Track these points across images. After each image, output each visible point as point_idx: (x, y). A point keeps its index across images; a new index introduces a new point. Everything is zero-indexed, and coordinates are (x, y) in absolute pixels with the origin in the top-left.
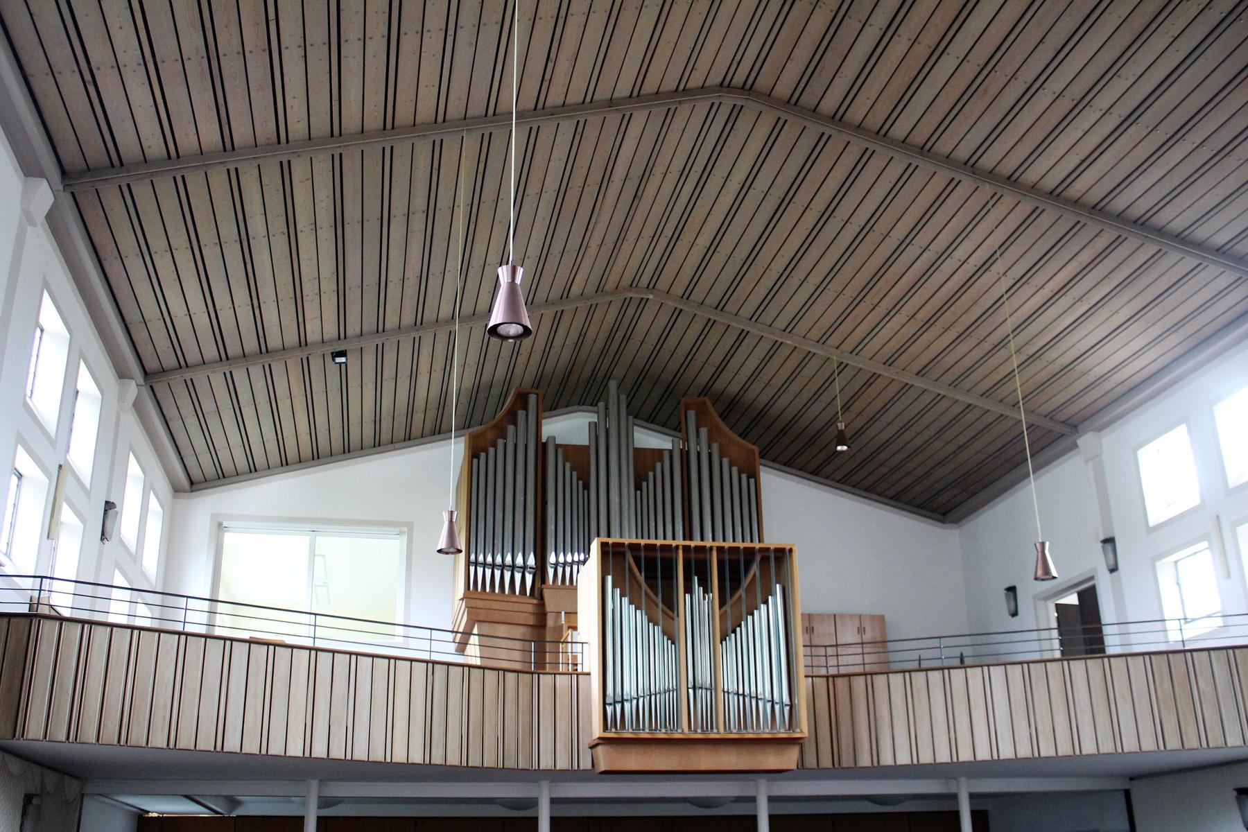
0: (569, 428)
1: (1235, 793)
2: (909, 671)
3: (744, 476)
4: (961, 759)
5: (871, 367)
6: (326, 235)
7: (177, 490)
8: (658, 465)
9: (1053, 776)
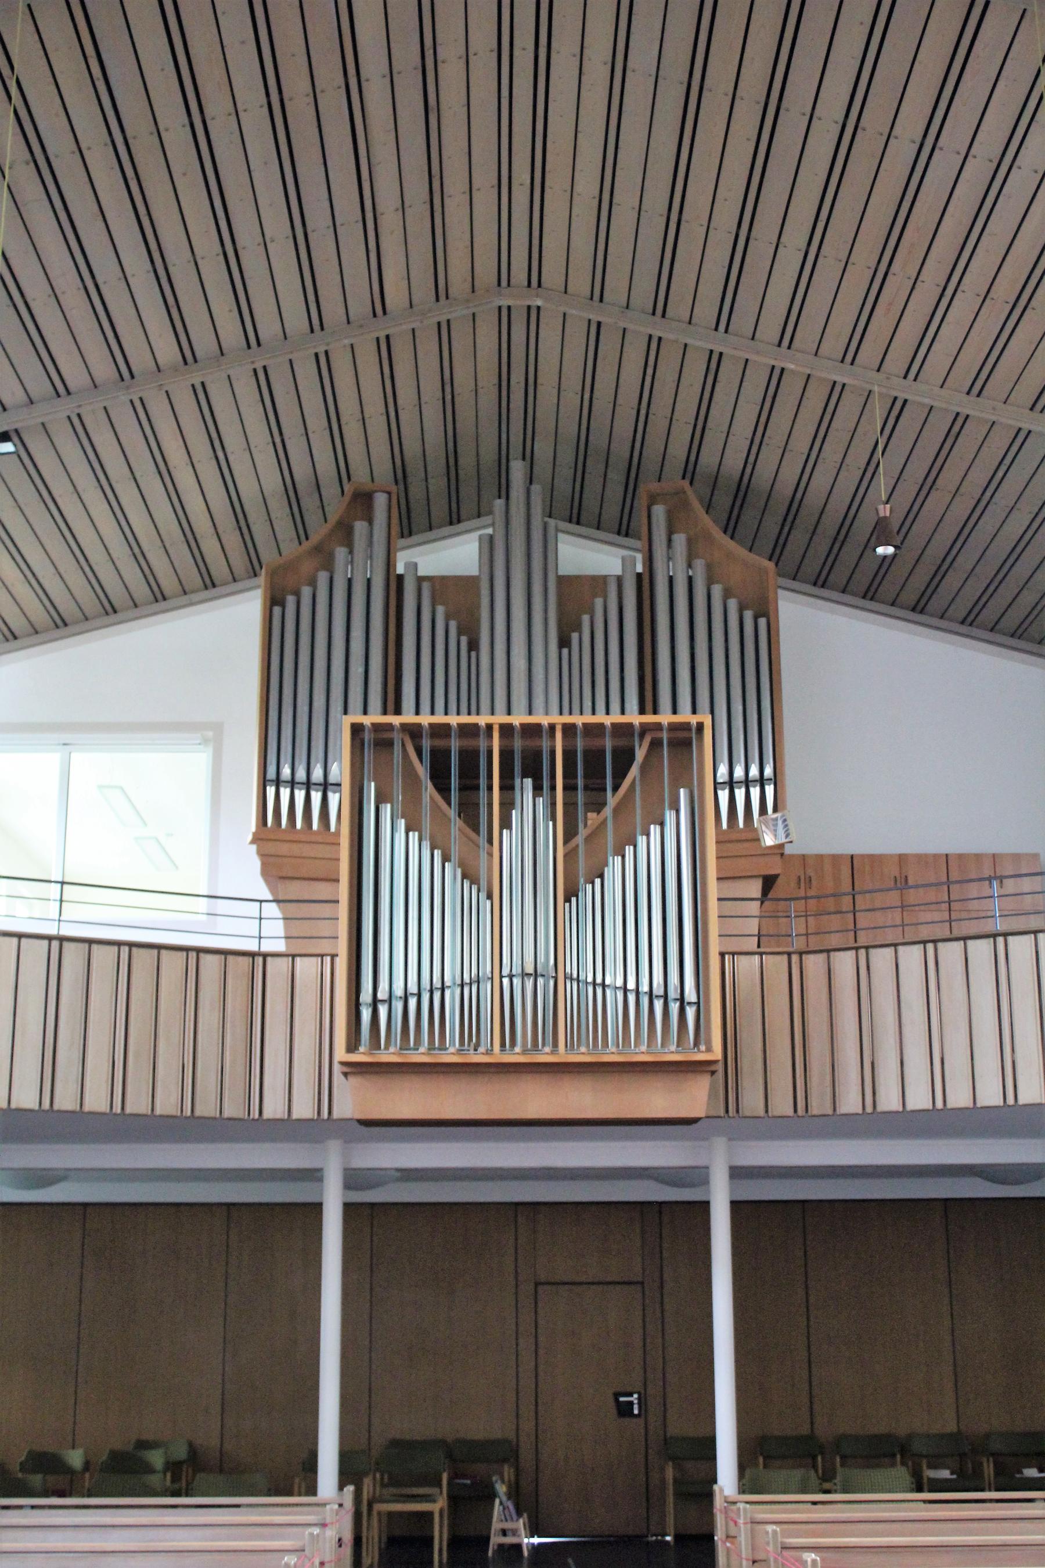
0: (456, 554)
3: (748, 615)
4: (1022, 1100)
5: (954, 401)
8: (599, 602)
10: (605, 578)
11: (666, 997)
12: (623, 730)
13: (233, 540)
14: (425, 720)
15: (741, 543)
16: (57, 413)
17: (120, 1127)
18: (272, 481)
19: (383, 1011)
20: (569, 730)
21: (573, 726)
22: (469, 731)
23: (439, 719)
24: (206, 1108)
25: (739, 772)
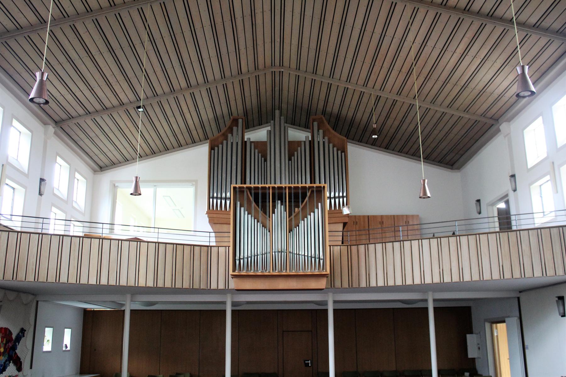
0: (259, 134)
1: (557, 299)
2: (403, 241)
3: (339, 152)
6: (107, 55)
7: (95, 171)
8: (299, 148)
9: (475, 291)
10: (301, 142)
11: (315, 257)
12: (304, 188)
13: (200, 131)
14: (252, 186)
15: (338, 133)
16: (154, 102)
17: (174, 291)
18: (211, 116)
19: (242, 261)
20: (290, 188)
21: (291, 187)
22: (264, 188)
23: (256, 185)
24: (196, 286)
25: (337, 195)
